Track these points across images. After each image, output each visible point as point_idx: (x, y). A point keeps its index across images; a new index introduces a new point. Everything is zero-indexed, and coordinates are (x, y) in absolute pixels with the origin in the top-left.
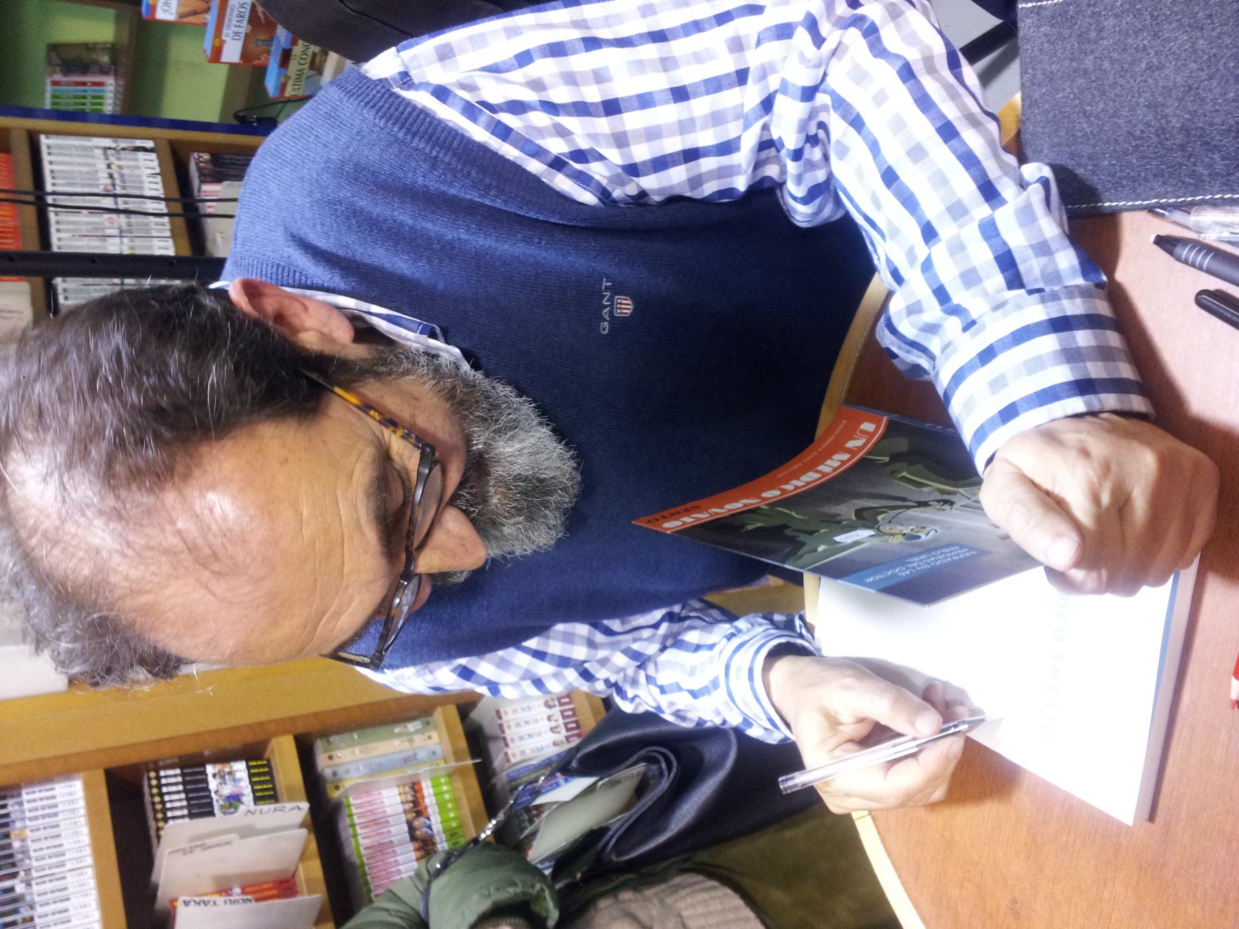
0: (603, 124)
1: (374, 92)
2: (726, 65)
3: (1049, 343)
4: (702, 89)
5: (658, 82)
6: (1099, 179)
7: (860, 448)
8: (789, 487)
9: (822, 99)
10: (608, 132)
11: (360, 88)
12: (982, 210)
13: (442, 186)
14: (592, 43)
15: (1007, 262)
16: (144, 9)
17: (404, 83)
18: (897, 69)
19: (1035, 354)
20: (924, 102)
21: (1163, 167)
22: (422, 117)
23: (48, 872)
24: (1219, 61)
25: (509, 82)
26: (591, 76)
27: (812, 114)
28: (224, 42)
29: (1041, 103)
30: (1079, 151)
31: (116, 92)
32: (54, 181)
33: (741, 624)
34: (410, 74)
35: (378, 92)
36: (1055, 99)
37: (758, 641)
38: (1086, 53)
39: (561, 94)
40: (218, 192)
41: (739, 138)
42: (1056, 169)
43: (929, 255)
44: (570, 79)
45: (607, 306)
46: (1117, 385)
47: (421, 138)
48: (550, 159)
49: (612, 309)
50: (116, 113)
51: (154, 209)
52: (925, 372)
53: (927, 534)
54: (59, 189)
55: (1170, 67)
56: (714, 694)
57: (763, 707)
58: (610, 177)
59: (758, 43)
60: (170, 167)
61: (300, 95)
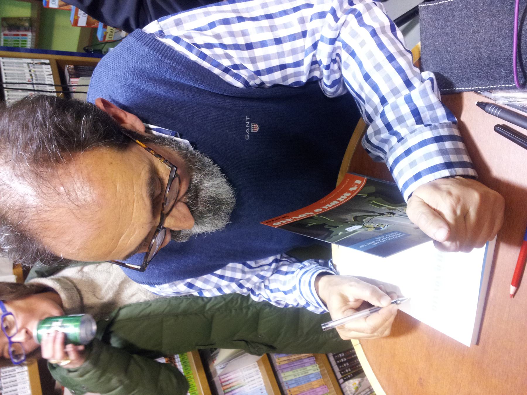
0: (246, 54)
1: (148, 39)
2: (297, 29)
3: (434, 147)
4: (288, 39)
5: (269, 36)
6: (454, 78)
7: (355, 191)
8: (326, 207)
9: (338, 44)
10: (248, 57)
11: (142, 37)
12: (405, 91)
13: (177, 79)
14: (241, 19)
15: (416, 113)
16: (44, 3)
17: (161, 35)
18: (370, 31)
19: (428, 152)
20: (381, 46)
21: (481, 73)
22: (169, 49)
23: (8, 374)
24: (502, 30)
25: (206, 35)
26: (240, 33)
27: (334, 50)
28: (79, 17)
29: (429, 46)
30: (445, 66)
31: (32, 39)
32: (6, 78)
33: (306, 263)
34: (163, 31)
35: (150, 39)
36: (435, 45)
37: (313, 270)
38: (447, 26)
39: (228, 41)
40: (77, 82)
41: (303, 60)
42: (436, 74)
43: (383, 110)
44: (232, 34)
45: (248, 128)
46: (462, 164)
47: (168, 59)
48: (223, 68)
49: (250, 129)
50: (32, 48)
51: (50, 89)
52: (382, 159)
53: (384, 227)
54: (9, 81)
55: (482, 32)
56: (294, 292)
57: (315, 298)
58: (249, 76)
59: (311, 20)
60: (57, 71)
61: (112, 40)
